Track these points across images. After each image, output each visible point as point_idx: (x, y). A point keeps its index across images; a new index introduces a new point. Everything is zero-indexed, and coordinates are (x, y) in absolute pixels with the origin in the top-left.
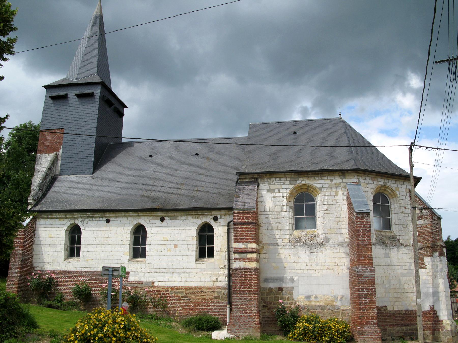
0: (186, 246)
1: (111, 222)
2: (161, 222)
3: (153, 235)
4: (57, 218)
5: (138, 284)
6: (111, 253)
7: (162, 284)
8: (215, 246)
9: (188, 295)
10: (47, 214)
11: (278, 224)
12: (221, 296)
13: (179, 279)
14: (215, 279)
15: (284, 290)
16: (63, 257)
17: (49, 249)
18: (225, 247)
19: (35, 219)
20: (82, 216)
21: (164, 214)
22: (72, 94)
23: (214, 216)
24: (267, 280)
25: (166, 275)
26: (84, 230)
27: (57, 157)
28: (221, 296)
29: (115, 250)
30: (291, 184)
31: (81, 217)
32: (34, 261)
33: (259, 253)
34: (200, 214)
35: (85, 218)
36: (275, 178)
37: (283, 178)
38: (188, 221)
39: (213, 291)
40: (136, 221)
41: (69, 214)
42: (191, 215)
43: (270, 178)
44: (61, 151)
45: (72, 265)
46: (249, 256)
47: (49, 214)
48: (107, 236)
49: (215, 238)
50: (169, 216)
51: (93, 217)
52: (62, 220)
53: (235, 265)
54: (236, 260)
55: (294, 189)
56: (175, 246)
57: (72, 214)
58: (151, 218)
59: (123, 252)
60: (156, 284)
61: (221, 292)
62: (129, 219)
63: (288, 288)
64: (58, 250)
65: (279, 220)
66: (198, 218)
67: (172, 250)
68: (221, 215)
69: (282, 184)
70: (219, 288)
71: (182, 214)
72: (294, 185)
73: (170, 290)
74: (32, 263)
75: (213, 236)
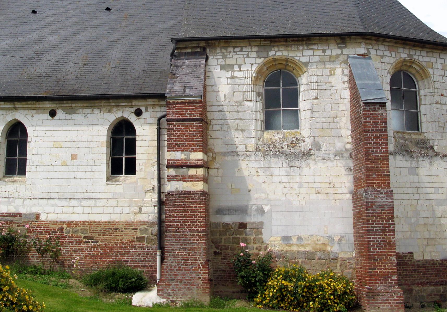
0: (90, 157)
2: (50, 118)
3: (38, 139)
7: (51, 218)
8: (138, 156)
9: (93, 235)
11: (238, 121)
12: (146, 236)
14: (137, 210)
15: (248, 226)
18: (153, 157)
21: (55, 105)
23: (135, 109)
24: (220, 211)
25: (58, 202)
28: (146, 236)
30: (259, 57)
33: (208, 168)
34: (113, 104)
36: (234, 47)
37: (246, 47)
38: (93, 116)
39: (134, 229)
40: (10, 117)
42: (100, 107)
43: (226, 48)
49: (138, 144)
50: (63, 109)
53: (170, 187)
54: (170, 179)
56: (74, 157)
58: (34, 112)
60: (43, 217)
61: (147, 229)
63: (254, 223)
65: (240, 115)
66: (109, 112)
67: (69, 162)
69: (245, 56)
70: (144, 223)
71: (85, 105)
72: (265, 58)
73: (65, 226)
75: (135, 140)
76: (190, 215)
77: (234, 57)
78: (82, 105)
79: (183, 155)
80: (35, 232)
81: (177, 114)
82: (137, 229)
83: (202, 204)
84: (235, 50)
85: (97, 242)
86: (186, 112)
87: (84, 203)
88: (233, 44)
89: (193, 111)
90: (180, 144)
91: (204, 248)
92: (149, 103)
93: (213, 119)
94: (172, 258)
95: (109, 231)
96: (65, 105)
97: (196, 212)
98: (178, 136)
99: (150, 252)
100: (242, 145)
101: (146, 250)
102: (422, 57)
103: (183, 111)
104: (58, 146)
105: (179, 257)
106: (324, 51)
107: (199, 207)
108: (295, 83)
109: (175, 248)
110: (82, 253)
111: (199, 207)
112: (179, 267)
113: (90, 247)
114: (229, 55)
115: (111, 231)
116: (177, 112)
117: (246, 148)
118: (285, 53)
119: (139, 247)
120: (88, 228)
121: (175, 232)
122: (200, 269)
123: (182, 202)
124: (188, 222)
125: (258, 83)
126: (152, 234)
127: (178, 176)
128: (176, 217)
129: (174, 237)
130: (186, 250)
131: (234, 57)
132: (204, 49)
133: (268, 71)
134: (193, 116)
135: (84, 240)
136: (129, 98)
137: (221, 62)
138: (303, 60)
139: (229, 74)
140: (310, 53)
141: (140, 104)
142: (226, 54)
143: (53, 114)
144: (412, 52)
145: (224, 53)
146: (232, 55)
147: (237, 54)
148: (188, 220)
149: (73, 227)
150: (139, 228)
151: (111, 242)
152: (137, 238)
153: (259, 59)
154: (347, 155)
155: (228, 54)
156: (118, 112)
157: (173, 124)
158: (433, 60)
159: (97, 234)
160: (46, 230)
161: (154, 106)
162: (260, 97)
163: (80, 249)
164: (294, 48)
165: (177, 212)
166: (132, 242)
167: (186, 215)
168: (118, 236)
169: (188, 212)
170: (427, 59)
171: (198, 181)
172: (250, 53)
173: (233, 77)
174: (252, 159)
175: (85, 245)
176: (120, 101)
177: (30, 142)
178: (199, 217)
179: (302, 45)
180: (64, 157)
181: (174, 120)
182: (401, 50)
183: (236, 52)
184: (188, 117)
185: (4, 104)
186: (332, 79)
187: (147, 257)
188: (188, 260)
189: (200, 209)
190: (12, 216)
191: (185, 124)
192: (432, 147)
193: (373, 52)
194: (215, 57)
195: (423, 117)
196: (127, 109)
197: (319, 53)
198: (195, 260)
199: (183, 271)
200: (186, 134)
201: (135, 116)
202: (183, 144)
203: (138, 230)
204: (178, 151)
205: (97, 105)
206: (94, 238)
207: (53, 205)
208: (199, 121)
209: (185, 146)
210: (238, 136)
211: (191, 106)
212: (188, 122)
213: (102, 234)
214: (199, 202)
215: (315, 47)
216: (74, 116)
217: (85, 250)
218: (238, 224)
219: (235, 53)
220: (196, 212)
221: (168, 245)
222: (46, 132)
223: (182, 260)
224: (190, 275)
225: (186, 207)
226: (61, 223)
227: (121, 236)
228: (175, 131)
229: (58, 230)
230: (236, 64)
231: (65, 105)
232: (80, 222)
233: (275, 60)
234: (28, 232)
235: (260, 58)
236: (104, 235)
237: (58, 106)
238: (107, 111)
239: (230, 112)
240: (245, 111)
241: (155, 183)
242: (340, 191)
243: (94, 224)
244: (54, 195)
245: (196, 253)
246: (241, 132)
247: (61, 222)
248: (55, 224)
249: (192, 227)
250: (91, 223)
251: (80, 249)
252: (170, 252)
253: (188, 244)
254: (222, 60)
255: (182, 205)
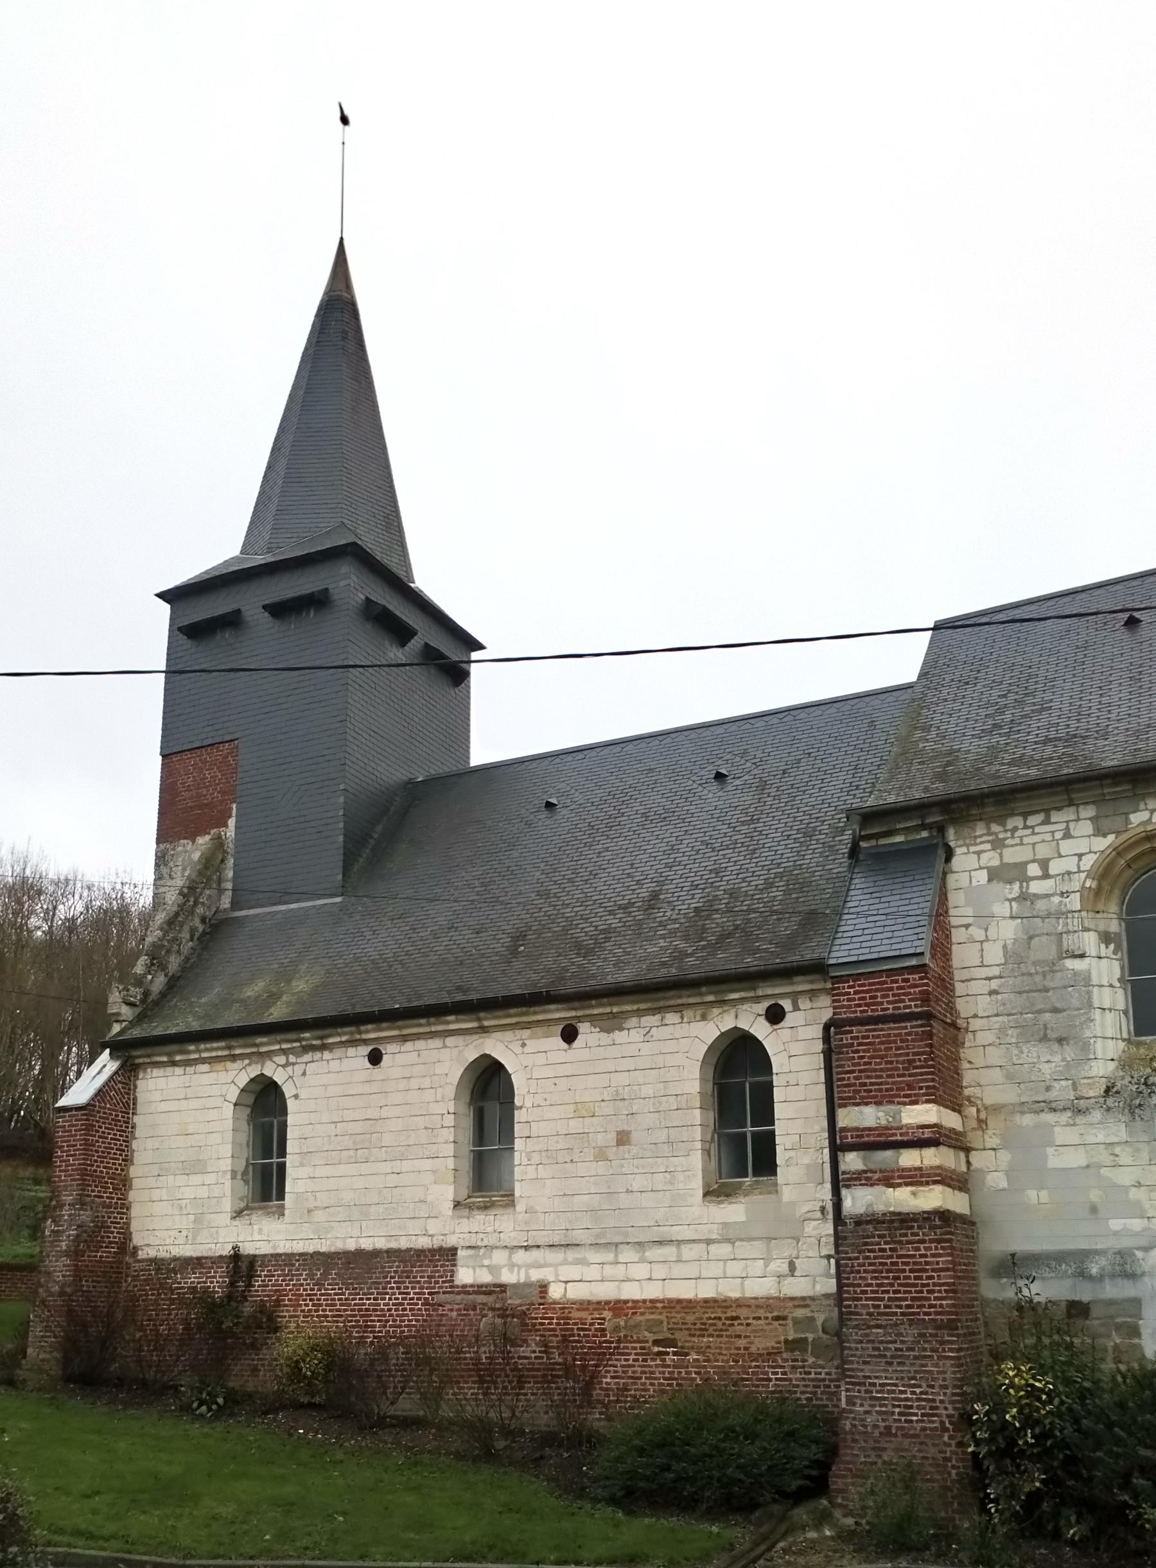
0: (662, 1136)
1: (386, 1059)
2: (565, 1045)
3: (538, 1100)
4: (203, 1061)
5: (490, 1293)
6: (393, 1180)
7: (577, 1292)
8: (779, 1128)
9: (678, 1335)
10: (168, 1049)
11: (1047, 1016)
12: (811, 1337)
13: (640, 1271)
14: (785, 1268)
15: (1095, 1312)
16: (227, 1205)
17: (181, 1180)
18: (817, 1128)
19: (129, 1072)
20: (284, 1046)
21: (573, 1013)
22: (251, 602)
23: (766, 1004)
24: (1013, 1265)
25: (594, 1256)
26: (296, 1096)
27: (219, 843)
28: (811, 1337)
29: (406, 1166)
30: (1099, 832)
31: (284, 1052)
32: (134, 1226)
33: (967, 1150)
34: (711, 998)
35: (298, 1055)
36: (1025, 815)
37: (1059, 809)
38: (664, 1032)
39: (777, 1318)
40: (470, 1050)
41: (241, 1041)
42: (679, 1009)
43: (1001, 820)
44: (232, 822)
45: (260, 1231)
46: (909, 1158)
47: (174, 1047)
48: (373, 1113)
49: (778, 1094)
50: (592, 1019)
51: (323, 1048)
52: (219, 1066)
53: (856, 1201)
54: (862, 1178)
55: (1119, 851)
56: (623, 1138)
57: (250, 1040)
58: (526, 1033)
59: (434, 1172)
60: (555, 1292)
61: (812, 1319)
62: (450, 1041)
63: (1111, 1302)
64: (210, 1179)
65: (1054, 998)
66: (704, 1018)
67: (611, 1153)
68: (794, 996)
69: (1058, 835)
70: (802, 1302)
71: (643, 1006)
72: (1118, 833)
73: (607, 1314)
74: (127, 1235)
75: (769, 1087)
76: (909, 1278)
77: (1025, 840)
78: (635, 1007)
79: (880, 1114)
80: (539, 1330)
81: (859, 1005)
82: (785, 1318)
83: (943, 1248)
84: (1029, 823)
85: (687, 1354)
86: (883, 997)
88: (1022, 806)
89: (904, 994)
90: (872, 1084)
91: (954, 1373)
92: (801, 988)
93: (975, 1016)
94: (865, 1399)
95: (715, 1325)
96: (596, 1011)
97: (926, 1271)
98: (865, 1064)
99: (824, 1380)
100: (1063, 1083)
101: (813, 1376)
103: (876, 997)
104: (586, 1114)
105: (884, 1399)
107: (933, 1256)
109: (872, 1371)
110: (651, 1384)
111: (933, 1256)
112: (885, 1427)
113: (669, 1366)
114: (1013, 837)
115: (719, 1323)
116: (860, 999)
117: (1075, 1089)
119: (793, 1367)
120: (663, 1317)
121: (869, 1327)
122: (946, 1435)
123: (886, 1243)
124: (906, 1299)
125: (1100, 907)
126: (824, 1331)
127: (872, 1171)
128: (870, 1285)
129: (869, 1342)
130: (902, 1378)
131: (1025, 840)
132: (941, 829)
133: (1131, 872)
134: (906, 1007)
135: (656, 1349)
136: (749, 978)
137: (991, 858)
141: (777, 991)
142: (1001, 836)
143: (569, 1035)
145: (996, 834)
146: (1021, 837)
147: (1034, 833)
148: (905, 1292)
149: (626, 1315)
150: (790, 1315)
151: (720, 1354)
152: (786, 1341)
153: (1100, 839)
155: (1009, 834)
156: (726, 1016)
157: (852, 1032)
159: (687, 1332)
160: (565, 1324)
162: (1112, 946)
163: (645, 1373)
165: (874, 1271)
166: (775, 1354)
167: (899, 1278)
168: (739, 1336)
169: (904, 1271)
171: (927, 1183)
172: (1072, 825)
173: (1023, 897)
174: (1095, 1120)
175: (658, 1362)
176: (724, 987)
177: (521, 1108)
178: (934, 1285)
180: (600, 1140)
183: (1032, 827)
184: (891, 1011)
185: (457, 1021)
187: (815, 1393)
188: (911, 1407)
189: (938, 1263)
190: (485, 1293)
191: (881, 1030)
194: (972, 849)
196: (745, 1007)
198: (932, 1408)
199: (900, 1439)
200: (886, 1056)
201: (767, 1024)
202: (881, 1084)
203: (790, 1322)
204: (867, 1104)
205: (671, 1002)
206: (680, 1344)
208: (921, 1019)
209: (887, 1090)
210: (1049, 1057)
211: (896, 981)
212: (892, 1025)
213: (698, 1333)
214: (931, 1241)
217: (658, 1375)
218: (1064, 1305)
219: (1029, 831)
220: (926, 1271)
221: (852, 1362)
222: (556, 1080)
223: (894, 1406)
224: (920, 1451)
225: (899, 1257)
226: (600, 1305)
227: (746, 1337)
228: (857, 1051)
229: (592, 1324)
230: (1033, 861)
231: (596, 1011)
232: (644, 1301)
234: (523, 1331)
235: (1105, 835)
236: (703, 1336)
237: (580, 1013)
238: (698, 1018)
239: (1020, 993)
240: (1066, 987)
243: (678, 1307)
244: (579, 1236)
245: (933, 1387)
246: (1056, 1047)
247: (599, 1303)
248: (584, 1310)
249: (918, 1314)
251: (645, 1373)
252: (859, 1384)
253: (907, 1362)
254: (991, 854)
255: (884, 1250)
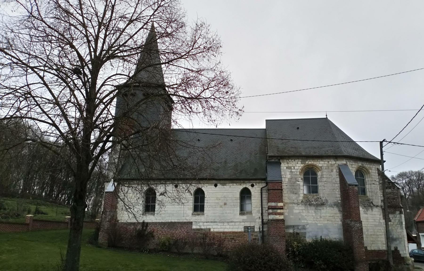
0: (232, 204)
7: (216, 230)
25: (219, 224)
30: (302, 164)
36: (292, 159)
38: (234, 187)
50: (220, 183)
56: (225, 204)
63: (302, 233)
66: (240, 185)
67: (223, 206)
73: (222, 234)
87: (230, 224)
102: (367, 165)
106: (328, 162)
108: (316, 174)
118: (312, 162)
132: (279, 160)
136: (249, 180)
137: (287, 165)
138: (320, 165)
139: (290, 170)
140: (323, 162)
143: (216, 186)
144: (363, 163)
154: (339, 205)
158: (371, 166)
161: (259, 183)
164: (316, 160)
170: (369, 166)
173: (291, 172)
179: (319, 159)
180: (221, 204)
181: (271, 189)
182: (359, 162)
186: (332, 173)
192: (372, 202)
193: (348, 163)
195: (367, 190)
197: (327, 163)
207: (216, 225)
215: (325, 160)
216: (225, 187)
226: (220, 232)
233: (308, 165)
241: (260, 215)
242: (337, 220)
250: (233, 233)
